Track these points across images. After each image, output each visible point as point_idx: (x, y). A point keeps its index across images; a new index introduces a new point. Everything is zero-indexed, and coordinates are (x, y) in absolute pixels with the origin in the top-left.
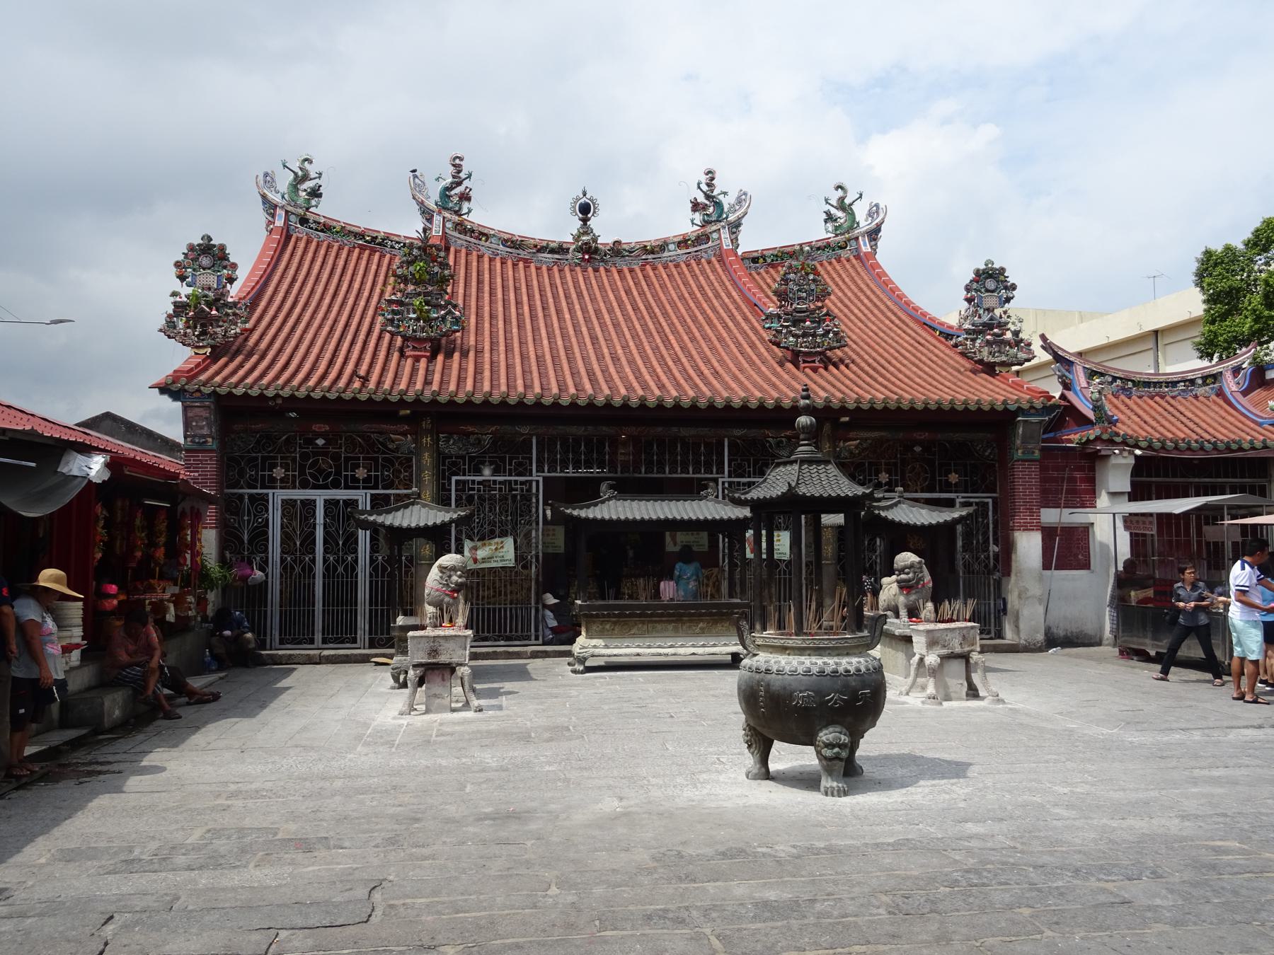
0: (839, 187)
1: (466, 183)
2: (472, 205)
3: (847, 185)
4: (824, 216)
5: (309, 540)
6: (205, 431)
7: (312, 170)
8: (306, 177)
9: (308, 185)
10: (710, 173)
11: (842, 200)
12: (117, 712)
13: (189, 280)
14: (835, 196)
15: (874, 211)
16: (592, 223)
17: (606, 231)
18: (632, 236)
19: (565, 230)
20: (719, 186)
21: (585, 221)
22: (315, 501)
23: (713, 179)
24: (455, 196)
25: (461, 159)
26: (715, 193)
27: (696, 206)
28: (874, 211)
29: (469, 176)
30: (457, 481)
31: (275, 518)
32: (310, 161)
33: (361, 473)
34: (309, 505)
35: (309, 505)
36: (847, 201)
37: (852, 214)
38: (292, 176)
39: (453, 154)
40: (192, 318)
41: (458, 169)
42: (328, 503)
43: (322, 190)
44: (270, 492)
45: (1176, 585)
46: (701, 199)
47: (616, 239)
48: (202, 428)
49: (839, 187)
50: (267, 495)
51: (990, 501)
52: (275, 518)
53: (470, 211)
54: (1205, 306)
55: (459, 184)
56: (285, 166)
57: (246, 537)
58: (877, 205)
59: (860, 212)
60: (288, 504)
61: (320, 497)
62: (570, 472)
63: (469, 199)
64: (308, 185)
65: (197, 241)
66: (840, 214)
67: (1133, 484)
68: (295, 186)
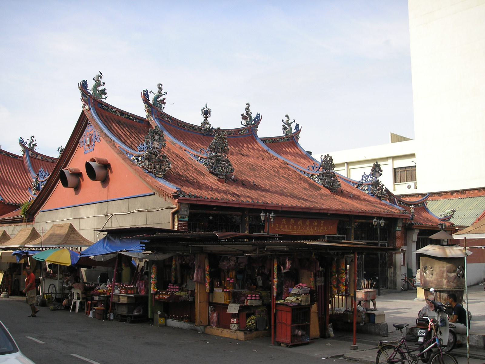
3: (250, 104)
6: (186, 213)
7: (102, 81)
11: (288, 121)
12: (266, 318)
14: (286, 119)
15: (297, 127)
17: (215, 123)
19: (197, 120)
20: (251, 109)
21: (206, 118)
27: (244, 117)
28: (297, 127)
36: (290, 122)
39: (160, 83)
40: (244, 134)
45: (170, 284)
47: (219, 127)
53: (164, 108)
54: (318, 157)
59: (293, 126)
67: (418, 238)
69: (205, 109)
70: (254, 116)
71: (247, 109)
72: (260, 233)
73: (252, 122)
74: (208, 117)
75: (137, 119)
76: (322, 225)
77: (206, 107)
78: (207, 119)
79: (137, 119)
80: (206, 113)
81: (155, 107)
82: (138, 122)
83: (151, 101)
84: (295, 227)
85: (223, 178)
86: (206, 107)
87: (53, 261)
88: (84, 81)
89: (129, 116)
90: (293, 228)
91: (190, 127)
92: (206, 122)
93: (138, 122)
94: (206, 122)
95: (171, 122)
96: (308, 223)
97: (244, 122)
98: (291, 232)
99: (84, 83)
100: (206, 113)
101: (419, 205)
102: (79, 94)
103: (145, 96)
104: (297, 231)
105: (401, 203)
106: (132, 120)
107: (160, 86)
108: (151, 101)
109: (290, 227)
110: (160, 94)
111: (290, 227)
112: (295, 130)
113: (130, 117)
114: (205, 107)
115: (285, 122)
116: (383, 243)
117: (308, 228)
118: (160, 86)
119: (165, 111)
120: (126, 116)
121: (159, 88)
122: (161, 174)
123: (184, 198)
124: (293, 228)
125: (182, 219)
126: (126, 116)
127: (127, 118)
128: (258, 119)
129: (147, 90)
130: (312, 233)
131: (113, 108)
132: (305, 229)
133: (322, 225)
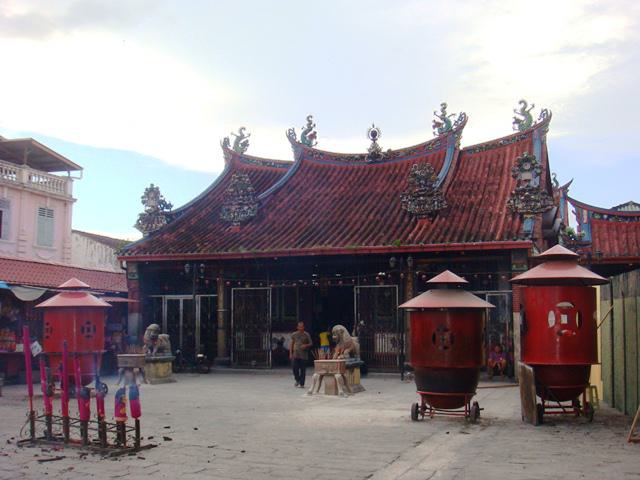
0: (520, 103)
1: (314, 130)
2: (317, 140)
5: (178, 316)
6: (135, 271)
7: (245, 133)
8: (242, 137)
9: (242, 141)
10: (444, 106)
17: (386, 144)
18: (395, 147)
20: (449, 112)
21: (374, 140)
23: (445, 108)
27: (437, 125)
31: (165, 308)
34: (178, 301)
35: (178, 301)
37: (531, 117)
41: (310, 122)
42: (184, 301)
46: (439, 120)
49: (520, 103)
52: (165, 308)
60: (170, 301)
61: (181, 298)
62: (247, 288)
64: (242, 141)
65: (149, 187)
66: (522, 118)
68: (237, 143)
70: (453, 120)
73: (449, 132)
80: (374, 135)
83: (299, 138)
92: (375, 145)
94: (375, 145)
97: (516, 126)
100: (374, 135)
103: (291, 136)
119: (318, 147)
121: (241, 133)
128: (463, 121)
131: (253, 159)
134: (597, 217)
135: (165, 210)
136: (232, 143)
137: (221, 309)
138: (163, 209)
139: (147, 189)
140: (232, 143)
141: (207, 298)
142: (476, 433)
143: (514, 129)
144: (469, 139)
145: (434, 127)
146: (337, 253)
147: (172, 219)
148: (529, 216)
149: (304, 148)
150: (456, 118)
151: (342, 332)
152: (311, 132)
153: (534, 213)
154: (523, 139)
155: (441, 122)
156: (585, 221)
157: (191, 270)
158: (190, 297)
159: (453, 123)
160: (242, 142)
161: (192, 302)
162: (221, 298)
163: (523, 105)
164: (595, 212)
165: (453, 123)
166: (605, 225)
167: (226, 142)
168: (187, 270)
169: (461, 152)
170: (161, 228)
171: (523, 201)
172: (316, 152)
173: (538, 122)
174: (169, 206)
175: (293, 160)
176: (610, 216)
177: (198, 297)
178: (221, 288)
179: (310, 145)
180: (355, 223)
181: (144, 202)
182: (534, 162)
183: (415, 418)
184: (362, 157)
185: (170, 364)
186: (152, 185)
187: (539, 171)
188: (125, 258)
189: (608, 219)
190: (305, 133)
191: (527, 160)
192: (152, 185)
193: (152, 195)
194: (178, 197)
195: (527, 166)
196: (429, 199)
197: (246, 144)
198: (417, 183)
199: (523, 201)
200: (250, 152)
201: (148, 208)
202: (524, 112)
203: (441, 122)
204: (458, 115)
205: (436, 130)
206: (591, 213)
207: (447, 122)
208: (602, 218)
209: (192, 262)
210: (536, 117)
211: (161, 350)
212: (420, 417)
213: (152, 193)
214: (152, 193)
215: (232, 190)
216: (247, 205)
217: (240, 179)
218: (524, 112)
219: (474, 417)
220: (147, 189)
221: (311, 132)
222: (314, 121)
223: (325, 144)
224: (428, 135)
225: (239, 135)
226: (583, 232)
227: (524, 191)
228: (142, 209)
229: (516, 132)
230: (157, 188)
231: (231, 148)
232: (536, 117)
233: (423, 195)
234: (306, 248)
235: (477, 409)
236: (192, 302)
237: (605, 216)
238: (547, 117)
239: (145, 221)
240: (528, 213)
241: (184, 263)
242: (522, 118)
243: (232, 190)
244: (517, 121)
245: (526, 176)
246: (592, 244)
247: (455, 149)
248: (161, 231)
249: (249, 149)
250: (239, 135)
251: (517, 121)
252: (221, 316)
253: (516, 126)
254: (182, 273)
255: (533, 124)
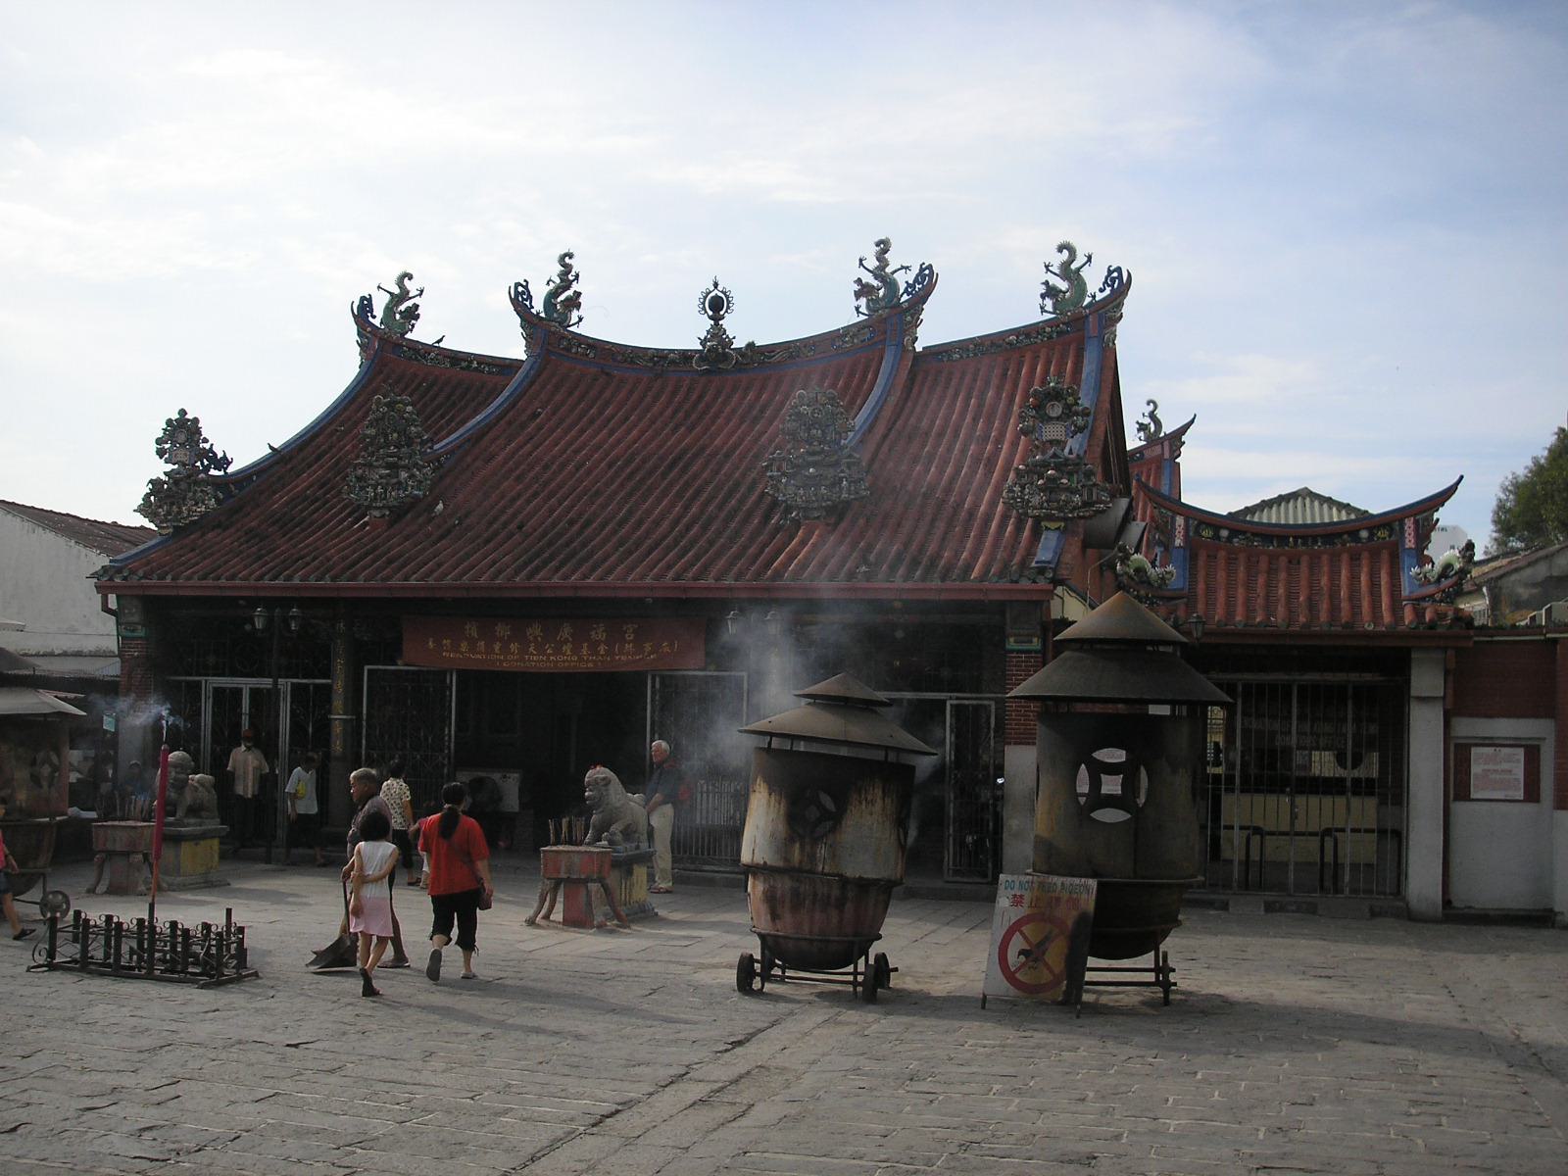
0: (1060, 249)
1: (575, 287)
2: (582, 312)
3: (877, 240)
4: (1043, 289)
6: (136, 619)
7: (412, 287)
8: (404, 295)
9: (402, 308)
10: (884, 246)
13: (167, 456)
14: (1058, 259)
16: (728, 323)
17: (744, 329)
19: (686, 333)
20: (894, 260)
21: (716, 318)
22: (241, 689)
23: (885, 251)
24: (565, 297)
25: (571, 256)
26: (888, 270)
27: (864, 290)
29: (577, 277)
30: (368, 670)
31: (207, 707)
32: (410, 277)
33: (211, 659)
34: (237, 693)
35: (237, 693)
38: (388, 297)
41: (567, 268)
43: (581, 300)
44: (202, 679)
46: (868, 278)
48: (132, 615)
49: (1060, 249)
50: (200, 682)
51: (993, 703)
55: (568, 287)
56: (861, 264)
57: (310, 730)
58: (1119, 270)
60: (219, 692)
61: (246, 684)
63: (578, 306)
64: (402, 308)
65: (175, 416)
66: (1063, 285)
68: (389, 310)
69: (713, 294)
70: (903, 279)
71: (881, 257)
72: (396, 665)
73: (893, 306)
74: (723, 318)
75: (495, 366)
76: (630, 637)
77: (716, 285)
78: (720, 322)
79: (495, 366)
80: (717, 306)
81: (548, 322)
82: (498, 373)
83: (538, 306)
84: (514, 647)
85: (383, 516)
86: (716, 285)
87: (1411, 788)
88: (363, 298)
89: (471, 362)
90: (505, 649)
91: (651, 359)
92: (717, 333)
93: (498, 373)
94: (717, 333)
95: (592, 355)
96: (566, 631)
98: (501, 661)
99: (365, 302)
100: (717, 306)
101: (1364, 534)
102: (352, 328)
103: (520, 299)
104: (522, 660)
105: (1224, 533)
106: (480, 371)
107: (565, 260)
108: (538, 306)
109: (497, 647)
110: (566, 284)
111: (497, 647)
112: (1101, 290)
113: (475, 365)
114: (712, 288)
115: (1057, 271)
116: (975, 702)
117: (567, 648)
118: (565, 260)
119: (582, 330)
120: (464, 364)
121: (564, 265)
122: (167, 527)
123: (108, 583)
124: (505, 649)
125: (129, 634)
126: (464, 364)
127: (469, 367)
128: (926, 282)
129: (525, 281)
130: (590, 665)
132: (558, 651)
133: (630, 637)
134: (1207, 533)
135: (213, 472)
136: (379, 310)
137: (338, 716)
138: (207, 469)
139: (169, 422)
140: (379, 310)
141: (307, 686)
142: (875, 1022)
143: (1043, 310)
144: (934, 329)
145: (858, 295)
146: (570, 594)
147: (229, 495)
148: (1053, 525)
149: (548, 322)
150: (911, 277)
151: (607, 782)
152: (569, 293)
153: (1065, 519)
154: (1060, 333)
155: (875, 283)
156: (1178, 542)
157: (270, 621)
158: (266, 683)
159: (902, 287)
160: (403, 308)
161: (273, 694)
162: (339, 686)
163: (1066, 252)
164: (1201, 523)
165: (902, 287)
166: (1222, 554)
167: (365, 307)
168: (259, 624)
169: (918, 358)
170: (203, 516)
171: (1041, 489)
172: (420, 350)
173: (1099, 296)
174: (225, 462)
175: (524, 357)
176: (1234, 533)
177: (285, 684)
178: (339, 666)
179: (564, 321)
180: (657, 523)
181: (160, 453)
182: (1070, 400)
183: (744, 984)
184: (685, 356)
185: (216, 842)
186: (183, 412)
187: (1080, 421)
188: (113, 589)
189: (1229, 539)
190: (553, 295)
191: (1056, 395)
192: (183, 412)
193: (182, 438)
194: (243, 439)
195: (1056, 410)
196: (830, 472)
197: (412, 314)
198: (804, 435)
199: (1041, 489)
200: (422, 333)
201: (170, 467)
202: (1068, 272)
203: (875, 283)
204: (916, 270)
205: (863, 301)
206: (1193, 523)
207: (889, 283)
208: (1217, 536)
209: (270, 603)
210: (1094, 282)
211: (194, 811)
212: (757, 984)
213: (182, 434)
214: (182, 434)
215: (371, 431)
216: (407, 468)
217: (391, 405)
218: (1068, 272)
219: (876, 987)
220: (169, 422)
221: (569, 293)
222: (577, 264)
223: (594, 322)
224: (842, 312)
225: (396, 290)
226: (1170, 568)
227: (1046, 465)
228: (160, 469)
229: (863, 317)
230: (196, 420)
231: (377, 322)
232: (1094, 282)
233: (814, 464)
234: (535, 581)
235: (882, 970)
236: (273, 694)
237: (1224, 533)
238: (1119, 284)
239: (160, 498)
240: (1050, 518)
241: (253, 602)
242: (1063, 285)
243: (371, 431)
244: (1050, 292)
245: (1053, 431)
246: (1190, 599)
247: (904, 349)
248: (203, 524)
249: (418, 324)
250: (396, 290)
251: (1050, 292)
252: (337, 729)
253: (1049, 303)
254: (248, 627)
255: (1088, 300)
